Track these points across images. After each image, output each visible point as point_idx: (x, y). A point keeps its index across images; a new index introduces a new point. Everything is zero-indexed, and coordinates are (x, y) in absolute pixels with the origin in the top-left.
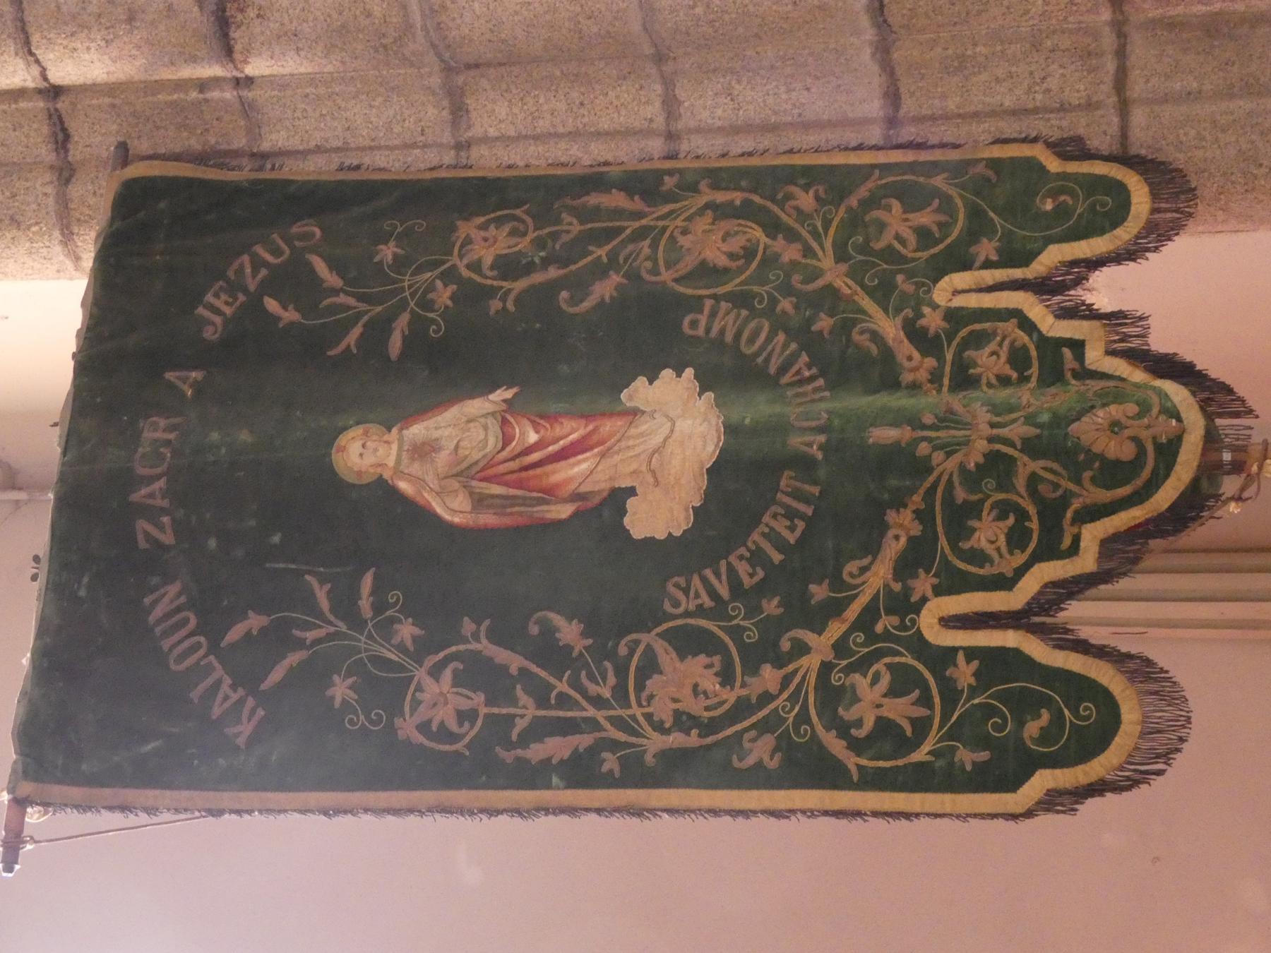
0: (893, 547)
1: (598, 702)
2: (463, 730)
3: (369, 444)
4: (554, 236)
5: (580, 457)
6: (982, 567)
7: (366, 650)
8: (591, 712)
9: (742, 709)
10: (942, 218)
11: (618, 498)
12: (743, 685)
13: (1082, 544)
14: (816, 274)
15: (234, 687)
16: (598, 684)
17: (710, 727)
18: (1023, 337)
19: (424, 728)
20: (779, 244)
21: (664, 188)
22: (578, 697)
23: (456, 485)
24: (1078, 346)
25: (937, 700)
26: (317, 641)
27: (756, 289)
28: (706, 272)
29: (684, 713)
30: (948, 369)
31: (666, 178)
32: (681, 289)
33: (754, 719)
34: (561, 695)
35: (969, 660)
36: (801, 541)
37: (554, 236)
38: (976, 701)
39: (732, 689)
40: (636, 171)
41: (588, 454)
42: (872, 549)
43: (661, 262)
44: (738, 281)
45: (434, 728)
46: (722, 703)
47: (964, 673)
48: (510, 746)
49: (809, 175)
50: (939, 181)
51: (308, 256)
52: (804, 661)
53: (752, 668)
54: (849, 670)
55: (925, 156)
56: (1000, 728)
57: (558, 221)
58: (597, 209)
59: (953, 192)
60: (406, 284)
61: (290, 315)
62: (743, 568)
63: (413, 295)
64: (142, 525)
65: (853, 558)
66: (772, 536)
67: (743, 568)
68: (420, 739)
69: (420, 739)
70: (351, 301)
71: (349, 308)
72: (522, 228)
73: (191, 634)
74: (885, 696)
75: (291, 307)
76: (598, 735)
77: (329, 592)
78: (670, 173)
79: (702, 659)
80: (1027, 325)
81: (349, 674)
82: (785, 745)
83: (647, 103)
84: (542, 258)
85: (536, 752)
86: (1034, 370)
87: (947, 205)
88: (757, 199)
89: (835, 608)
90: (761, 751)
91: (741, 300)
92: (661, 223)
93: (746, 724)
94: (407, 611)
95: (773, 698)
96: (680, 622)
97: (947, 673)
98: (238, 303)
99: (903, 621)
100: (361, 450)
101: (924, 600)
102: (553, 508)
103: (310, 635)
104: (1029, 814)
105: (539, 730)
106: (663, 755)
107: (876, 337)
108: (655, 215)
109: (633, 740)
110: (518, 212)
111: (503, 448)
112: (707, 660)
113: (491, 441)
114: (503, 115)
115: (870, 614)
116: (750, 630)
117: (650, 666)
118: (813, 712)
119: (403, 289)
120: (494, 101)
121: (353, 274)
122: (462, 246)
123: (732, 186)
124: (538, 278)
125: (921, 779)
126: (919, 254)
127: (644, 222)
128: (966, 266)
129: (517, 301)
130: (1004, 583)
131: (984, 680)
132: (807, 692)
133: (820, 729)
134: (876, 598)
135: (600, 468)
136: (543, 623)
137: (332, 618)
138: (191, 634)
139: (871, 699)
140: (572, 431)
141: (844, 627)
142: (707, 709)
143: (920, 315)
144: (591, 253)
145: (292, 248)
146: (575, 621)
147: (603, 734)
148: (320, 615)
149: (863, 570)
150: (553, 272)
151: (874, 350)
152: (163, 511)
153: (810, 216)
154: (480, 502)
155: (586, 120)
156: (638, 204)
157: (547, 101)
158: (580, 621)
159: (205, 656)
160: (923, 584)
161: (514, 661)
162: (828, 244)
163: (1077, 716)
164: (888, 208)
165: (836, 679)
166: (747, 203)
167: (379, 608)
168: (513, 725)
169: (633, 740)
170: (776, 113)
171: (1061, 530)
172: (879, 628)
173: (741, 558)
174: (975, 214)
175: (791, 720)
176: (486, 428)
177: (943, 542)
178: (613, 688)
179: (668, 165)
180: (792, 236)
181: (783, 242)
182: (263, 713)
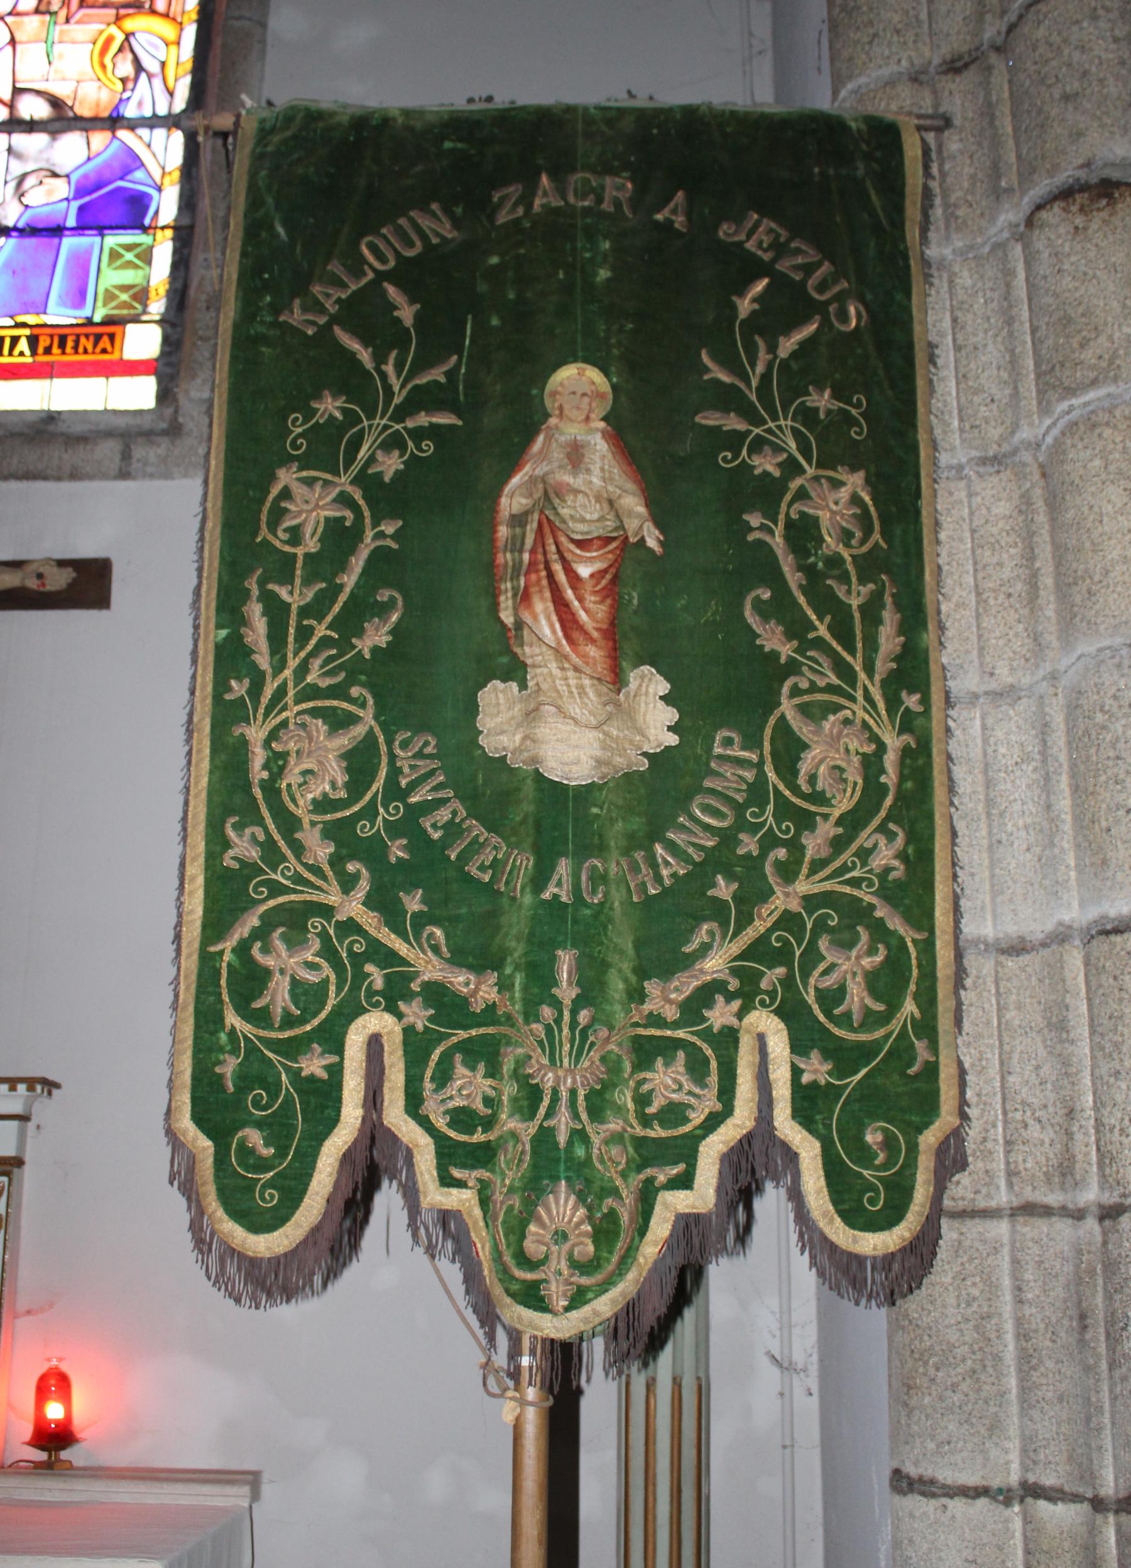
0: (460, 980)
1: (303, 670)
2: (280, 534)
3: (586, 400)
4: (844, 578)
5: (557, 626)
6: (432, 1079)
7: (370, 426)
8: (293, 663)
9: (289, 824)
10: (856, 1018)
11: (516, 671)
12: (313, 824)
13: (454, 1191)
14: (788, 873)
15: (339, 301)
16: (322, 667)
17: (271, 789)
18: (697, 1118)
19: (286, 494)
20: (826, 830)
21: (904, 694)
22: (309, 648)
23: (536, 496)
24: (685, 1182)
25: (287, 1034)
26: (384, 376)
27: (770, 807)
28: (789, 751)
29: (286, 762)
30: (669, 1033)
31: (916, 697)
32: (772, 721)
33: (277, 837)
34: (310, 631)
35: (327, 1068)
36: (468, 879)
37: (844, 578)
38: (284, 1077)
39: (309, 811)
40: (927, 663)
41: (560, 634)
42: (458, 958)
43: (806, 698)
44: (781, 787)
45: (283, 505)
46: (294, 800)
47: (314, 1065)
48: (262, 583)
49: (919, 858)
50: (909, 1007)
51: (818, 317)
52: (335, 887)
53: (330, 832)
54: (324, 935)
55: (943, 990)
56: (257, 1104)
57: (862, 581)
58: (879, 621)
59: (895, 1026)
60: (782, 422)
61: (745, 306)
62: (443, 815)
63: (769, 431)
64: (514, 190)
65: (448, 936)
66: (476, 847)
67: (443, 815)
68: (275, 491)
69: (275, 491)
70: (760, 368)
71: (753, 365)
72: (854, 542)
73: (397, 253)
74: (293, 978)
75: (756, 306)
76: (270, 671)
77: (436, 382)
78: (925, 701)
79: (341, 779)
80: (713, 1122)
81: (344, 410)
82: (249, 869)
83: (1012, 669)
84: (815, 565)
85: (255, 611)
86: (657, 1132)
87: (871, 1020)
88: (888, 801)
89: (393, 916)
90: (243, 847)
91: (758, 792)
92: (859, 695)
93: (272, 827)
94: (413, 463)
95: (298, 857)
96: (383, 748)
97: (315, 1045)
98: (760, 253)
99: (377, 993)
100: (580, 392)
101: (400, 1016)
102: (510, 602)
103: (389, 368)
104: (171, 1134)
105: (276, 611)
106: (244, 742)
107: (705, 950)
108: (870, 687)
109: (261, 711)
110: (876, 536)
111: (573, 541)
112: (340, 783)
113: (581, 527)
114: (995, 511)
115: (388, 958)
116: (371, 828)
117: (339, 722)
118: (281, 899)
119: (775, 418)
120: (1009, 499)
121: (794, 366)
122: (830, 479)
123: (906, 772)
124: (787, 564)
125: (208, 1019)
126: (812, 991)
127: (862, 676)
128: (798, 1047)
129: (760, 543)
130: (414, 1103)
131: (307, 1086)
132: (302, 892)
133: (263, 908)
134: (404, 962)
135: (544, 648)
136: (391, 605)
137: (409, 386)
138: (397, 253)
139: (289, 963)
140: (591, 613)
141: (373, 932)
142: (289, 785)
143: (730, 997)
144: (821, 619)
145: (827, 303)
146: (390, 638)
147: (269, 678)
148: (413, 373)
149: (436, 950)
150: (793, 579)
151: (688, 949)
152: (529, 206)
153: (864, 864)
154: (519, 520)
155: (992, 602)
156: (883, 666)
157: (1012, 557)
158: (388, 643)
159: (374, 270)
160: (417, 1014)
161: (349, 580)
162: (827, 886)
163: (265, 1187)
164: (872, 951)
165: (316, 923)
166: (883, 790)
167: (418, 434)
168: (282, 583)
169: (261, 711)
170: (1001, 814)
171: (473, 1167)
172: (369, 968)
173: (454, 813)
174: (866, 1052)
175: (274, 876)
176: (602, 519)
177: (463, 1034)
178: (316, 685)
179: (936, 697)
180: (838, 844)
181: (832, 834)
182: (310, 332)
